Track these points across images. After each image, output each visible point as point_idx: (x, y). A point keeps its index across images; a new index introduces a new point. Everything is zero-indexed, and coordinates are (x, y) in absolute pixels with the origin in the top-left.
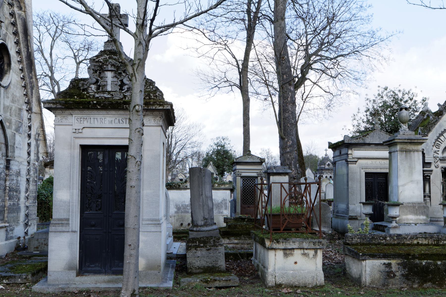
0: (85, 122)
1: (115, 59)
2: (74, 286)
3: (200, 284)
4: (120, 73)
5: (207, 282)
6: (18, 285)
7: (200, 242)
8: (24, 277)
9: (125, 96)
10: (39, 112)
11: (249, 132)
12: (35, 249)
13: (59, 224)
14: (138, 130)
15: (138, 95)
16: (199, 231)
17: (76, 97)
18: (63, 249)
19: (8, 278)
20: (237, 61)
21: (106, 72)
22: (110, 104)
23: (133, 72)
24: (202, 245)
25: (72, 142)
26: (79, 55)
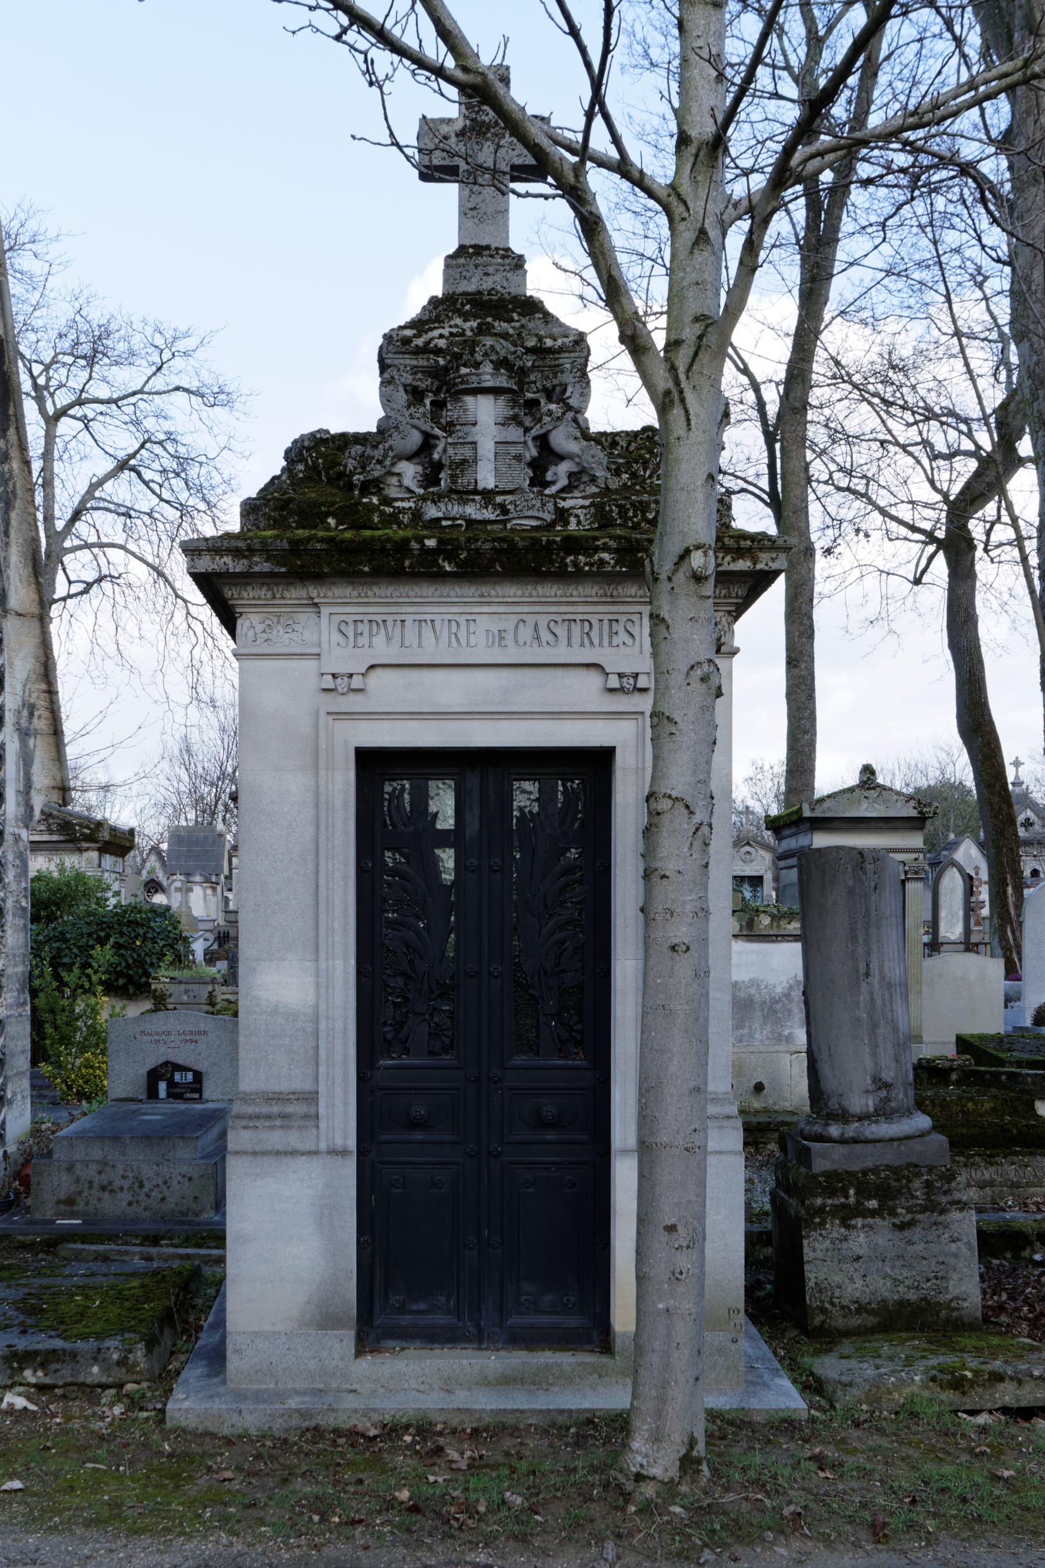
0: (380, 640)
1: (505, 336)
2: (351, 1402)
3: (926, 1394)
4: (534, 404)
5: (958, 1384)
6: (91, 1392)
7: (863, 1193)
8: (115, 1356)
9: (563, 515)
10: (35, 609)
11: (813, 690)
12: (63, 1207)
13: (269, 1117)
14: (699, 672)
15: (700, 496)
16: (855, 1141)
17: (331, 521)
18: (288, 1232)
19: (44, 1359)
20: (756, 387)
21: (469, 399)
22: (502, 551)
23: (670, 385)
24: (873, 1204)
25: (322, 734)
26: (54, 383)
